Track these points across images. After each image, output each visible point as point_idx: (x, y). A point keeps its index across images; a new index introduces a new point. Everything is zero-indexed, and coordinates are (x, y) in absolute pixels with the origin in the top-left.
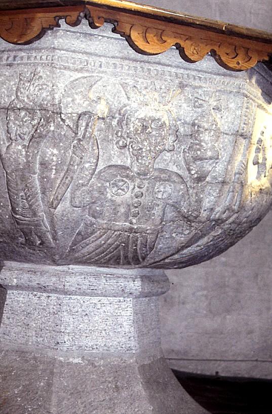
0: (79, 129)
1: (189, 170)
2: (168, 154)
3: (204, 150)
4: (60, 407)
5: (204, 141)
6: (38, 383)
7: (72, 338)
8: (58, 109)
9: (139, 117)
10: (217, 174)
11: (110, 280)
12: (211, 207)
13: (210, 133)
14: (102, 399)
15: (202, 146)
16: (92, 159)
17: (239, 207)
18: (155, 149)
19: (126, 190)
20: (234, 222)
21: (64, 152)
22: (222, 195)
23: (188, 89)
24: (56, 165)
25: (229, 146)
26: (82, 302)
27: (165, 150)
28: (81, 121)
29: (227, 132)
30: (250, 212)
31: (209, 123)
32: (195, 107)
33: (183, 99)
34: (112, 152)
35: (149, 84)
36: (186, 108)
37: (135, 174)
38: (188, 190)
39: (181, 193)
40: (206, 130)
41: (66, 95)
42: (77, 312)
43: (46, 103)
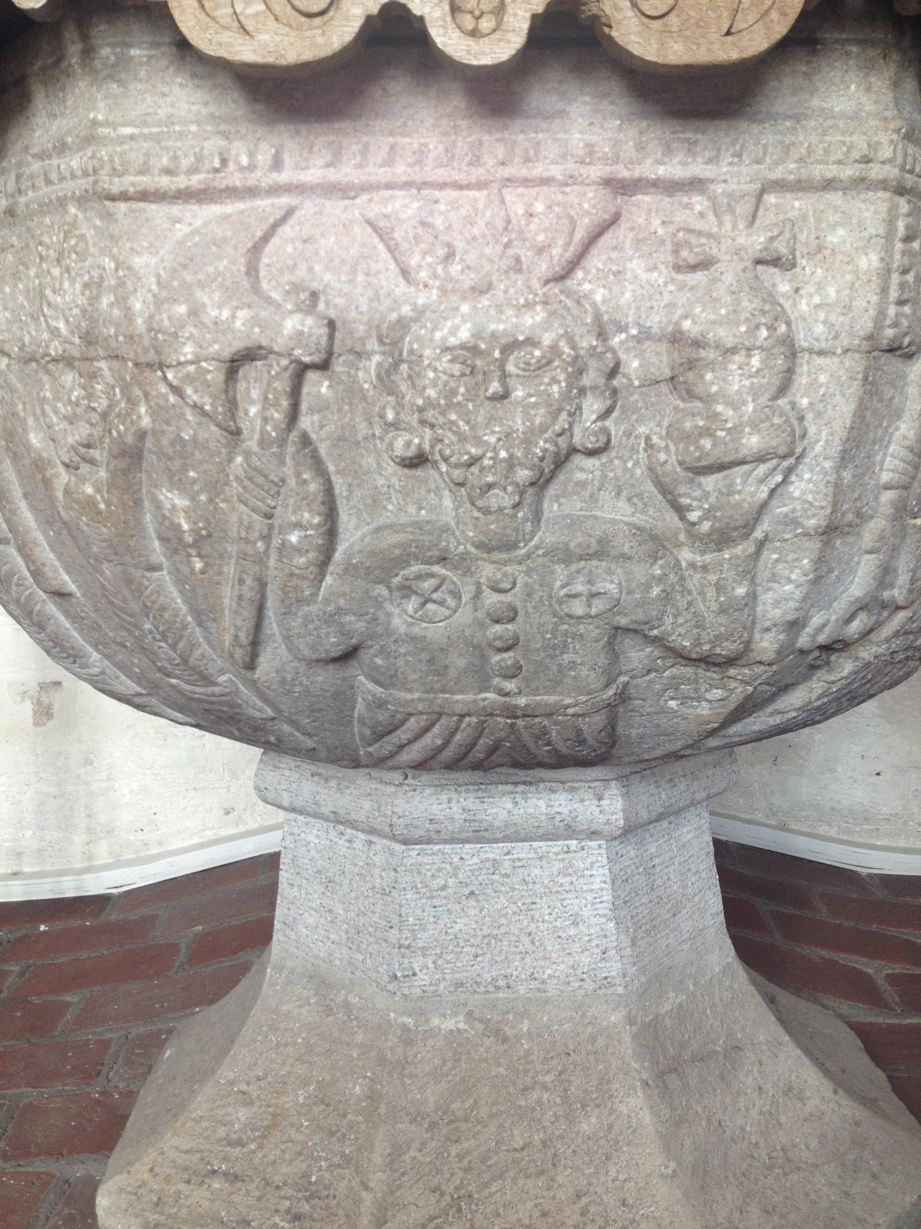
0: (241, 413)
1: (680, 510)
2: (591, 463)
3: (729, 431)
4: (396, 1170)
5: (722, 396)
6: (350, 1085)
7: (434, 962)
8: (152, 351)
9: (453, 341)
11: (526, 799)
14: (521, 1144)
16: (306, 515)
18: (527, 452)
20: (897, 634)
21: (211, 500)
22: (830, 571)
23: (647, 198)
26: (456, 859)
27: (573, 450)
28: (241, 386)
29: (824, 345)
31: (738, 324)
32: (678, 268)
33: (628, 242)
35: (481, 206)
36: (644, 276)
37: (473, 550)
38: (682, 578)
42: (444, 887)
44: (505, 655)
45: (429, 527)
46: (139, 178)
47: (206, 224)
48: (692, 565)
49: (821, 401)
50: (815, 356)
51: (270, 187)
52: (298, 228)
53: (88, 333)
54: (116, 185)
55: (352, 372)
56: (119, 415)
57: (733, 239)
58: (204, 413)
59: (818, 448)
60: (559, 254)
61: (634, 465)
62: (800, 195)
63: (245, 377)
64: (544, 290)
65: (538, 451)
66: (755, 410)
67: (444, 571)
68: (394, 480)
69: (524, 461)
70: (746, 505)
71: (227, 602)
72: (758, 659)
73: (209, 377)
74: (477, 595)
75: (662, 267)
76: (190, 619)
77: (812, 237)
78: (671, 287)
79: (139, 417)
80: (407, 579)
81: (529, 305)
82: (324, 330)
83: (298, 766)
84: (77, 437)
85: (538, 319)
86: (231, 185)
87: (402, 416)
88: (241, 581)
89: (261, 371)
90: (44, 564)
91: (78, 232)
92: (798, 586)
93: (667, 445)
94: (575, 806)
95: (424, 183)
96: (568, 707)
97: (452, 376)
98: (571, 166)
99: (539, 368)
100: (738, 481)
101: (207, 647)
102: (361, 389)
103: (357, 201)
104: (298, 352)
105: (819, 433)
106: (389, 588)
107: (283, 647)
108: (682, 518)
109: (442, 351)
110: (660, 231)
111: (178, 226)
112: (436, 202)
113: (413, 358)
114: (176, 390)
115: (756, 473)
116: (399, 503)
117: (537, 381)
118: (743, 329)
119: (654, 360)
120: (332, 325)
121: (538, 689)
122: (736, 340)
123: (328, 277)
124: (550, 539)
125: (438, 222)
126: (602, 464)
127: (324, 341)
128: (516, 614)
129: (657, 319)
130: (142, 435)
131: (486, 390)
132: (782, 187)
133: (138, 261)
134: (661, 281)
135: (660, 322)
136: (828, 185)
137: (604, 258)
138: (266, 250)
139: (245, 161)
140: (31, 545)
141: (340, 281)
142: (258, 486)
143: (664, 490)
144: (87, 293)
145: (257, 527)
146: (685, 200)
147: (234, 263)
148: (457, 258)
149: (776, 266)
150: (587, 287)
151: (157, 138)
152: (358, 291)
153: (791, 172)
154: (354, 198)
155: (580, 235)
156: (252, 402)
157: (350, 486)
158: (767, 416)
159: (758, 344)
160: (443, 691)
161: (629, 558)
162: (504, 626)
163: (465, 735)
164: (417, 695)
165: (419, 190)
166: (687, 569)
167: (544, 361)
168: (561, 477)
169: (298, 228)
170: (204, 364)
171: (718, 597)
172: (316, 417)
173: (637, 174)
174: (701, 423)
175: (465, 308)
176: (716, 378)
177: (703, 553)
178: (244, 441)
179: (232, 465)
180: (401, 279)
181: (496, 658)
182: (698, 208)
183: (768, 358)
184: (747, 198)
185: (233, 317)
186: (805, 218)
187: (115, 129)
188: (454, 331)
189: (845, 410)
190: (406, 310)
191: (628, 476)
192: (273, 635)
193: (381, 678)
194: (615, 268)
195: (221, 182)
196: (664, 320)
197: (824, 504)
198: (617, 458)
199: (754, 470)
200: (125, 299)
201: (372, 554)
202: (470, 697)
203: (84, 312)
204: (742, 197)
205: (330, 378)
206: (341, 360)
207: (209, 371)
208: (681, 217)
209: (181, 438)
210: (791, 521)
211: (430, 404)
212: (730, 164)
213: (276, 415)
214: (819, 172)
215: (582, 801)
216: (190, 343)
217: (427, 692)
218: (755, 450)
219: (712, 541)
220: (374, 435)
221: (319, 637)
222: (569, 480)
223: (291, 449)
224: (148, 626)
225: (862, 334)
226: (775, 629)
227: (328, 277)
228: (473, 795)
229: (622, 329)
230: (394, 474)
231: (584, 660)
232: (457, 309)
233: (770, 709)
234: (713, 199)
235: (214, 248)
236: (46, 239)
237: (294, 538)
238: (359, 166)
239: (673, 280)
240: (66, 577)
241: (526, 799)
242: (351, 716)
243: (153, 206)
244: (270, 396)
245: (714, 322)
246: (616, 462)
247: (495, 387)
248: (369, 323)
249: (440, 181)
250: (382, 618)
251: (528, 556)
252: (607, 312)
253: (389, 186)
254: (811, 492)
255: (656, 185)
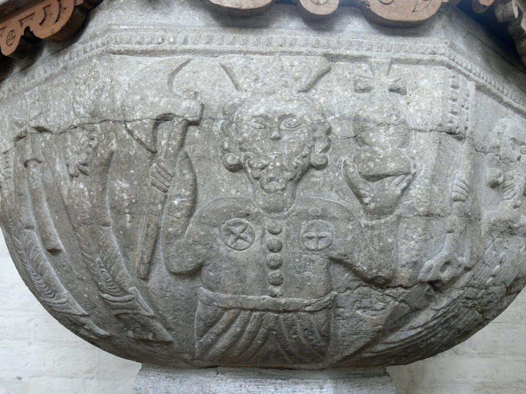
1: (360, 197)
2: (318, 173)
3: (380, 159)
5: (377, 143)
8: (122, 116)
9: (256, 113)
10: (414, 200)
11: (282, 387)
12: (414, 260)
13: (387, 129)
15: (375, 152)
16: (183, 190)
17: (471, 259)
18: (289, 163)
19: (249, 238)
23: (342, 63)
24: (128, 207)
25: (428, 152)
27: (311, 166)
28: (160, 131)
29: (421, 127)
30: (498, 267)
31: (383, 113)
32: (356, 91)
33: (335, 80)
34: (219, 177)
36: (341, 93)
37: (262, 211)
39: (349, 238)
40: (379, 125)
41: (131, 91)
43: (105, 109)
44: (275, 271)
45: (241, 200)
46: (127, 45)
47: (152, 64)
48: (367, 226)
49: (422, 152)
50: (417, 132)
51: (182, 50)
52: (191, 67)
53: (93, 112)
54: (116, 48)
55: (210, 127)
56: (103, 146)
57: (379, 80)
58: (142, 143)
59: (422, 173)
60: (305, 81)
61: (339, 174)
62: (407, 65)
63: (161, 128)
64: (298, 95)
65: (294, 163)
66: (392, 151)
67: (247, 222)
68: (225, 177)
69: (287, 168)
70: (390, 196)
71: (139, 239)
72: (400, 283)
73: (146, 126)
74: (263, 236)
75: (348, 89)
76: (119, 253)
77: (413, 82)
78: (353, 98)
79: (112, 145)
80: (229, 225)
81: (291, 100)
82: (200, 107)
83: (159, 374)
84: (80, 160)
85: (295, 106)
86: (165, 49)
87: (232, 147)
88: (148, 226)
89: (169, 125)
90: (50, 234)
91: (96, 70)
92: (417, 242)
93: (353, 165)
94: (308, 392)
95: (247, 51)
96: (306, 306)
97: (256, 128)
98: (309, 48)
99: (295, 127)
100: (387, 184)
101: (125, 269)
102: (214, 134)
103: (218, 58)
104: (186, 116)
105: (422, 166)
106: (220, 230)
107: (164, 267)
108: (362, 202)
109: (252, 118)
110: (348, 76)
111: (140, 65)
112: (252, 59)
113: (238, 120)
114: (130, 132)
115: (394, 181)
116: (227, 189)
117: (294, 133)
118: (385, 115)
119: (347, 128)
120: (203, 105)
121: (291, 293)
122: (383, 120)
123: (203, 87)
124: (299, 208)
125: (253, 67)
126: (324, 174)
127: (199, 113)
128: (282, 246)
129: (348, 111)
130: (112, 153)
131: (271, 135)
132: (399, 61)
133: (121, 79)
134: (349, 96)
135: (349, 112)
136: (418, 62)
137: (324, 85)
138: (177, 76)
139: (172, 40)
140: (46, 224)
141: (208, 89)
142: (162, 176)
143: (353, 186)
144: (96, 93)
145: (159, 197)
146: (359, 65)
147: (163, 79)
148: (260, 81)
149: (398, 93)
150: (317, 96)
151: (136, 30)
152: (216, 93)
153: (403, 56)
154: (216, 57)
155: (314, 74)
156: (163, 139)
157: (205, 179)
158: (398, 154)
159: (392, 122)
160: (243, 293)
161: (337, 219)
162: (275, 254)
163: (252, 324)
164: (229, 295)
165: (245, 54)
166: (365, 227)
167: (297, 124)
168: (305, 179)
169: (191, 67)
170: (144, 121)
171: (379, 243)
172: (192, 146)
173: (338, 53)
174: (369, 155)
175: (263, 100)
176: (374, 135)
177: (372, 220)
178: (158, 156)
179: (151, 167)
180: (235, 89)
181: (271, 273)
182: (364, 68)
183: (397, 129)
184: (384, 64)
185: (160, 101)
186: (410, 74)
187: (119, 26)
188: (257, 109)
189: (432, 156)
190: (236, 101)
191: (336, 180)
192: (160, 259)
193: (211, 284)
194: (329, 89)
195: (161, 47)
196: (351, 112)
197: (426, 200)
198: (331, 171)
199: (393, 180)
200: (113, 94)
201: (213, 212)
202: (256, 297)
203: (93, 102)
204: (383, 64)
205: (200, 129)
206: (205, 121)
207: (146, 124)
208: (357, 71)
209: (130, 154)
210: (411, 208)
211: (245, 140)
212: (377, 51)
213: (174, 143)
214: (414, 56)
215: (312, 389)
216: (139, 111)
217: (235, 293)
218: (393, 170)
219: (375, 213)
220: (218, 155)
221: (183, 258)
222: (309, 181)
223: (179, 159)
224: (98, 259)
225: (437, 123)
226: (407, 266)
227: (203, 87)
228: (254, 383)
229: (332, 114)
230: (226, 174)
231: (315, 273)
232: (259, 100)
233: (408, 326)
234: (370, 65)
235: (155, 73)
236: (80, 76)
237: (176, 202)
238: (220, 44)
239: (354, 96)
240: (60, 241)
241: (282, 387)
242: (193, 316)
243: (131, 57)
244: (172, 135)
245: (372, 112)
246: (330, 173)
247: (275, 134)
248: (219, 107)
249: (254, 51)
250: (215, 247)
251: (289, 215)
252: (326, 107)
253: (232, 52)
254: (420, 194)
255: (346, 57)
